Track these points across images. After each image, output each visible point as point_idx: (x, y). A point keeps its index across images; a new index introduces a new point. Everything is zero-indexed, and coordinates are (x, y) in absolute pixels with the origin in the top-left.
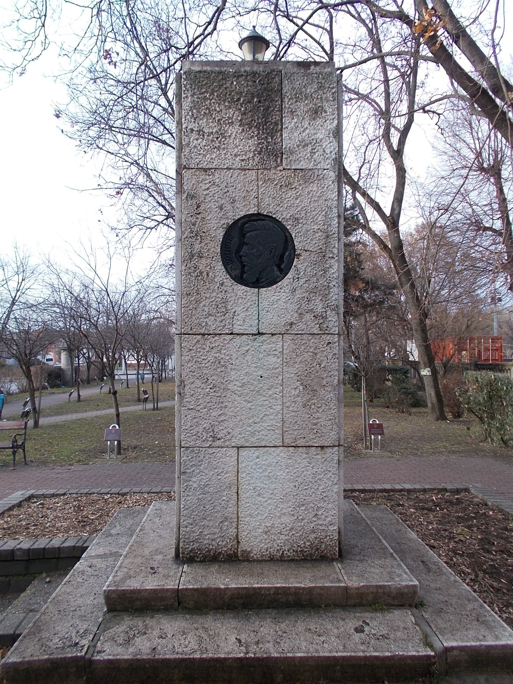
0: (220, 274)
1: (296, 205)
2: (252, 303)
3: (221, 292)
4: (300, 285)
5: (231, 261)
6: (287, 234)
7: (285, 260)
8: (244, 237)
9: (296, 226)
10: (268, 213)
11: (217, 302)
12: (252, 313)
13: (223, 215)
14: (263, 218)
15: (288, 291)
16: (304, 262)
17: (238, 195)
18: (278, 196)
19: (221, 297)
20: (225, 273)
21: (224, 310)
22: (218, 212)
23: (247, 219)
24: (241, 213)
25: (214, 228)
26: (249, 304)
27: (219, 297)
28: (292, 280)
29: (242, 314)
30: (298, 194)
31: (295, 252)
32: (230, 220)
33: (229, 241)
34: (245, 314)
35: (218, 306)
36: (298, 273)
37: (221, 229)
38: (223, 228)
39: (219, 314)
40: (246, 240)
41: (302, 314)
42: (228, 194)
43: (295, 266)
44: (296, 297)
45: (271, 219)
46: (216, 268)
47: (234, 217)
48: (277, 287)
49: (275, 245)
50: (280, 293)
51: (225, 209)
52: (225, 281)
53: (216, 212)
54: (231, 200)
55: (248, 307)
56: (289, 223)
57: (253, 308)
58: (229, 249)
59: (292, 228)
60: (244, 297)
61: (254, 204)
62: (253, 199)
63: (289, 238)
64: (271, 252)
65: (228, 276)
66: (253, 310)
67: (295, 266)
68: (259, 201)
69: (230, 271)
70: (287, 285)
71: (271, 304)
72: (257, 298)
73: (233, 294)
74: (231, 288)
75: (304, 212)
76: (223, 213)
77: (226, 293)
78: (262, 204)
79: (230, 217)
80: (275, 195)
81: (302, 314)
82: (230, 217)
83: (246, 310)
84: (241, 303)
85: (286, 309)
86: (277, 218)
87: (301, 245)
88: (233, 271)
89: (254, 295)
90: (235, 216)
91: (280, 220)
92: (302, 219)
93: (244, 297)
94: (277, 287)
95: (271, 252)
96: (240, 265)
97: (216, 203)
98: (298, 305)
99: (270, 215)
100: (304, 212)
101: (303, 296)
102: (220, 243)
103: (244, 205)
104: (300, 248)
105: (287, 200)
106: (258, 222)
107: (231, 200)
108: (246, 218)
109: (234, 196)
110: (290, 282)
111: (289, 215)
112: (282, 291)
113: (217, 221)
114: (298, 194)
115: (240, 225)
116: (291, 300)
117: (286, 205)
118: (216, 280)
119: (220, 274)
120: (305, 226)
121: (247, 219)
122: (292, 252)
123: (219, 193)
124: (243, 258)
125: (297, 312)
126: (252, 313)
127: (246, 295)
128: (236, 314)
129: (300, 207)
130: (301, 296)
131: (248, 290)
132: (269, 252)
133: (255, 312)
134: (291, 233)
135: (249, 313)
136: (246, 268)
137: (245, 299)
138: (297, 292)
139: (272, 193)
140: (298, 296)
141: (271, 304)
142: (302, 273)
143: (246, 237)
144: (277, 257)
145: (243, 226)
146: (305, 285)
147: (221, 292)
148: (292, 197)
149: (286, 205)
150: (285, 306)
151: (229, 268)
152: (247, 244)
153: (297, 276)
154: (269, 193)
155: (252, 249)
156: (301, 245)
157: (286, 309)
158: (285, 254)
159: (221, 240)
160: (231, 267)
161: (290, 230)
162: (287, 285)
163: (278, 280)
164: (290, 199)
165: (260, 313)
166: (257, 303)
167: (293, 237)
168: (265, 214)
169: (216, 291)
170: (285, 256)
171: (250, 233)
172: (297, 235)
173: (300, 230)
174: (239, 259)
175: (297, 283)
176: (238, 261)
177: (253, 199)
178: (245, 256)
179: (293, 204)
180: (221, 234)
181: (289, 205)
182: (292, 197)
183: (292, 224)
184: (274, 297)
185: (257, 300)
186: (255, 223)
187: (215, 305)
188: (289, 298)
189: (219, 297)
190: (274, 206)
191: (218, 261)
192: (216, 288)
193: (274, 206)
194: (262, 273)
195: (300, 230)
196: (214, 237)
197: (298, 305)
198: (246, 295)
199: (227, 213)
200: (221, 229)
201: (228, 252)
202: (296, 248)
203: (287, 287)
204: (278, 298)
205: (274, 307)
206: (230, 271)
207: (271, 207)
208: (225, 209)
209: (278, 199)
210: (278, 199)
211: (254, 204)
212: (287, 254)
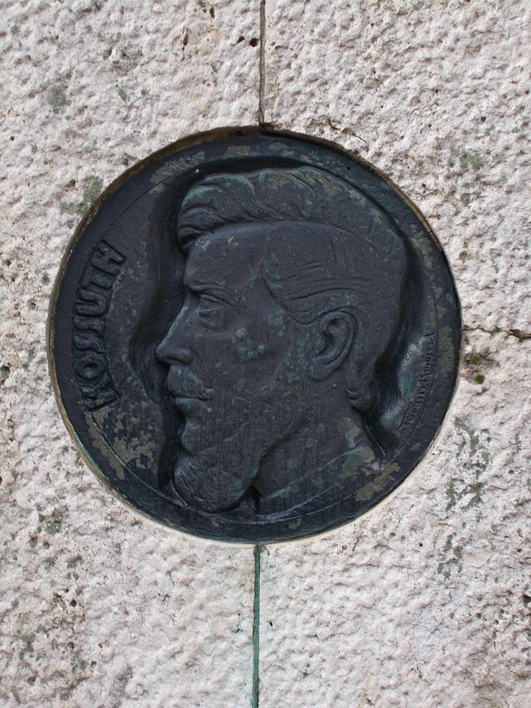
0: (46, 466)
1: (467, 83)
2: (222, 627)
3: (51, 562)
4: (485, 526)
5: (109, 385)
6: (417, 242)
7: (403, 384)
8: (185, 255)
9: (466, 198)
10: (313, 123)
11: (24, 618)
12: (221, 683)
13: (69, 134)
14: (287, 154)
15: (416, 560)
16: (508, 401)
17: (151, 25)
18: (374, 31)
19: (48, 593)
20: (71, 457)
21: (64, 665)
22: (41, 116)
23: (201, 156)
24: (167, 125)
25: (17, 209)
26: (205, 629)
27: (36, 594)
28: (442, 499)
29: (164, 690)
30: (481, 25)
31: (458, 347)
32: (103, 165)
33: (100, 279)
34: (180, 689)
35: (29, 640)
36: (477, 458)
37: (53, 211)
38: (64, 208)
39: (35, 689)
40: (190, 272)
41: (493, 686)
42: (95, 20)
43: (458, 422)
44: (462, 595)
45: (330, 159)
46: (20, 431)
47: (129, 149)
48: (359, 538)
49: (349, 299)
50: (375, 573)
51: (81, 100)
52: (71, 501)
53: (31, 116)
54: (115, 55)
55: (200, 650)
56: (430, 181)
57: (223, 655)
58: (96, 323)
59: (448, 208)
60: (176, 591)
61: (241, 78)
62: (233, 51)
63: (428, 263)
64: (329, 338)
65: (90, 477)
66: (223, 666)
67: (458, 422)
68: (269, 60)
69: (100, 443)
70: (413, 529)
71: (323, 631)
72: (248, 600)
73: (114, 577)
74: (104, 544)
75: (512, 124)
76: (64, 125)
77: (79, 569)
78: (283, 75)
79: (104, 148)
80: (355, 27)
81: (493, 686)
82: (104, 148)
83: (188, 665)
84: (158, 626)
85: (406, 659)
86: (366, 156)
87: (494, 303)
88: (120, 444)
89: (234, 581)
90: (131, 139)
91: (381, 165)
92: (499, 159)
93: (176, 591)
94: (359, 538)
95: (329, 338)
96: (157, 412)
97: (27, 68)
98: (471, 635)
99: (328, 135)
100: (512, 124)
101: (503, 585)
102: (48, 289)
103: (185, 83)
104: (489, 323)
105: (421, 54)
106: (262, 174)
107: (115, 55)
108: (193, 150)
109: (127, 30)
110: (430, 512)
111: (431, 138)
112: (388, 559)
113: (32, 171)
114: (481, 25)
115: (159, 189)
116: (435, 612)
117: (413, 83)
118: (20, 496)
119: (46, 466)
120: (516, 200)
121: (201, 156)
122: (446, 342)
123: (47, 15)
124: (176, 370)
125: (466, 673)
126: (221, 683)
127: (186, 583)
128: (130, 687)
129: (494, 98)
130: (490, 586)
131: (201, 555)
132: (319, 342)
133: (235, 678)
134: (442, 236)
135: (201, 685)
136: (191, 426)
137: (181, 601)
138: (467, 563)
139: (339, 18)
140: (475, 587)
141: (323, 631)
142: (498, 461)
143: (194, 254)
144: (361, 365)
145: (182, 195)
146: (512, 528)
147: (51, 562)
148: (448, 42)
149: (413, 83)
150: (404, 642)
151: (95, 431)
152: (196, 294)
153: (469, 477)
154: (325, 17)
155: (226, 324)
156: (494, 303)
157: (406, 659)
158: (404, 348)
159: (53, 273)
160: (109, 421)
161: (434, 224)
162: (413, 529)
163: (362, 495)
164: (437, 52)
165: (265, 680)
166: (247, 625)
167: (453, 257)
168: (299, 129)
169: (23, 559)
170: (406, 363)
171: (219, 235)
172: (473, 247)
173: (492, 220)
174: (156, 375)
175: (471, 513)
176: (150, 387)
177: (233, 51)
178: (184, 363)
179: (454, 77)
180: (56, 242)
181: (433, 83)
182: (448, 42)
183: (446, 186)
184: (340, 592)
185: (248, 612)
186: (242, 178)
187: (18, 635)
188: (425, 598)
189: (36, 594)
190: (349, 86)
191: (34, 392)
192: (22, 541)
193: (349, 86)
194: (279, 454)
195: (492, 220)
196: (15, 254)
197: (471, 635)
198: (186, 583)
199: (89, 123)
200: (53, 211)
201: (91, 340)
202: (467, 318)
203: (414, 538)
204: (365, 597)
205: (344, 649)
206: (100, 443)
207: (334, 91)
208: (81, 100)
209: (373, 51)
210: (373, 51)
211: (241, 78)
212: (413, 348)
